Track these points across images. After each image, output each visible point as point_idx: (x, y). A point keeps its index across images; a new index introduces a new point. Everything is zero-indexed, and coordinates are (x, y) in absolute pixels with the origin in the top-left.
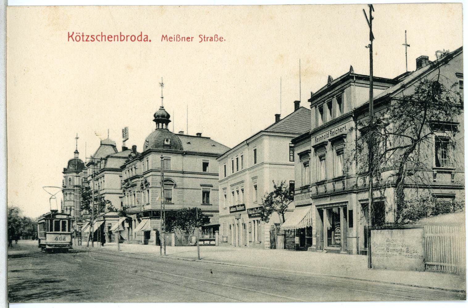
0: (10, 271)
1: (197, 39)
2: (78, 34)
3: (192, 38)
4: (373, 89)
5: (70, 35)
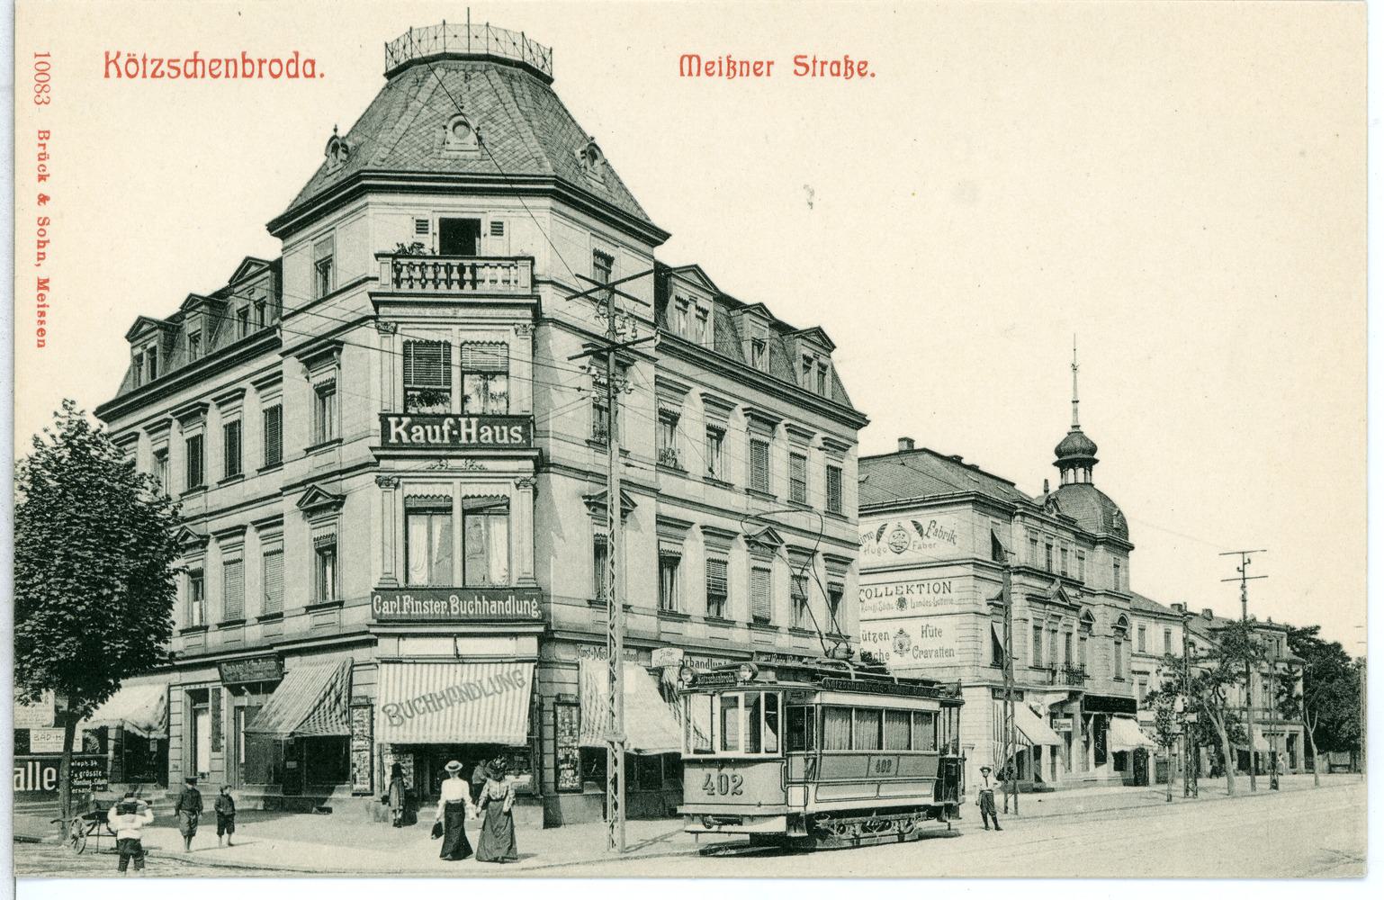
0: (1356, 816)
1: (784, 66)
2: (132, 57)
3: (769, 64)
4: (511, 413)
5: (112, 57)
